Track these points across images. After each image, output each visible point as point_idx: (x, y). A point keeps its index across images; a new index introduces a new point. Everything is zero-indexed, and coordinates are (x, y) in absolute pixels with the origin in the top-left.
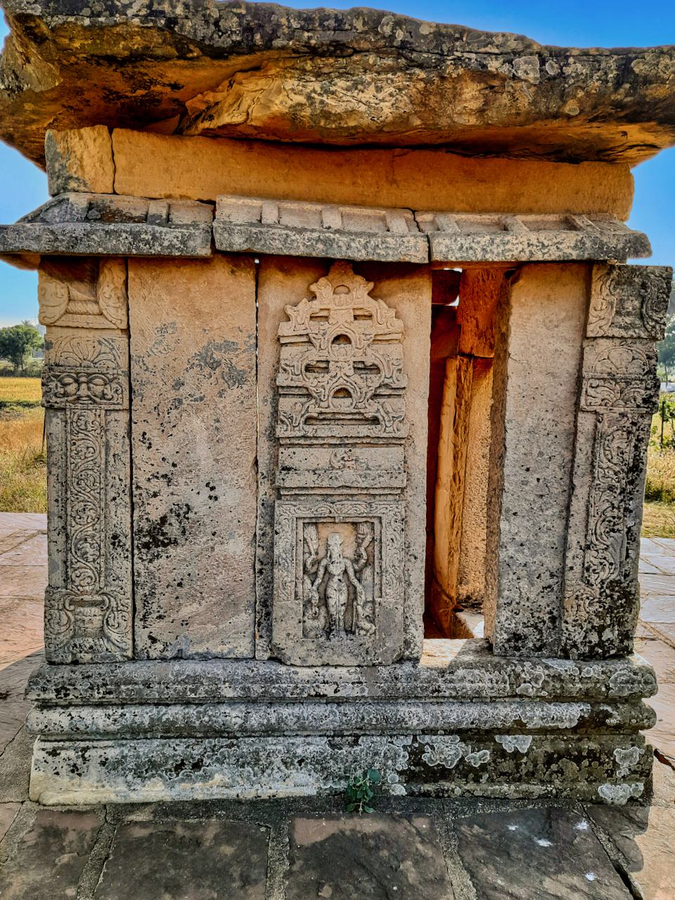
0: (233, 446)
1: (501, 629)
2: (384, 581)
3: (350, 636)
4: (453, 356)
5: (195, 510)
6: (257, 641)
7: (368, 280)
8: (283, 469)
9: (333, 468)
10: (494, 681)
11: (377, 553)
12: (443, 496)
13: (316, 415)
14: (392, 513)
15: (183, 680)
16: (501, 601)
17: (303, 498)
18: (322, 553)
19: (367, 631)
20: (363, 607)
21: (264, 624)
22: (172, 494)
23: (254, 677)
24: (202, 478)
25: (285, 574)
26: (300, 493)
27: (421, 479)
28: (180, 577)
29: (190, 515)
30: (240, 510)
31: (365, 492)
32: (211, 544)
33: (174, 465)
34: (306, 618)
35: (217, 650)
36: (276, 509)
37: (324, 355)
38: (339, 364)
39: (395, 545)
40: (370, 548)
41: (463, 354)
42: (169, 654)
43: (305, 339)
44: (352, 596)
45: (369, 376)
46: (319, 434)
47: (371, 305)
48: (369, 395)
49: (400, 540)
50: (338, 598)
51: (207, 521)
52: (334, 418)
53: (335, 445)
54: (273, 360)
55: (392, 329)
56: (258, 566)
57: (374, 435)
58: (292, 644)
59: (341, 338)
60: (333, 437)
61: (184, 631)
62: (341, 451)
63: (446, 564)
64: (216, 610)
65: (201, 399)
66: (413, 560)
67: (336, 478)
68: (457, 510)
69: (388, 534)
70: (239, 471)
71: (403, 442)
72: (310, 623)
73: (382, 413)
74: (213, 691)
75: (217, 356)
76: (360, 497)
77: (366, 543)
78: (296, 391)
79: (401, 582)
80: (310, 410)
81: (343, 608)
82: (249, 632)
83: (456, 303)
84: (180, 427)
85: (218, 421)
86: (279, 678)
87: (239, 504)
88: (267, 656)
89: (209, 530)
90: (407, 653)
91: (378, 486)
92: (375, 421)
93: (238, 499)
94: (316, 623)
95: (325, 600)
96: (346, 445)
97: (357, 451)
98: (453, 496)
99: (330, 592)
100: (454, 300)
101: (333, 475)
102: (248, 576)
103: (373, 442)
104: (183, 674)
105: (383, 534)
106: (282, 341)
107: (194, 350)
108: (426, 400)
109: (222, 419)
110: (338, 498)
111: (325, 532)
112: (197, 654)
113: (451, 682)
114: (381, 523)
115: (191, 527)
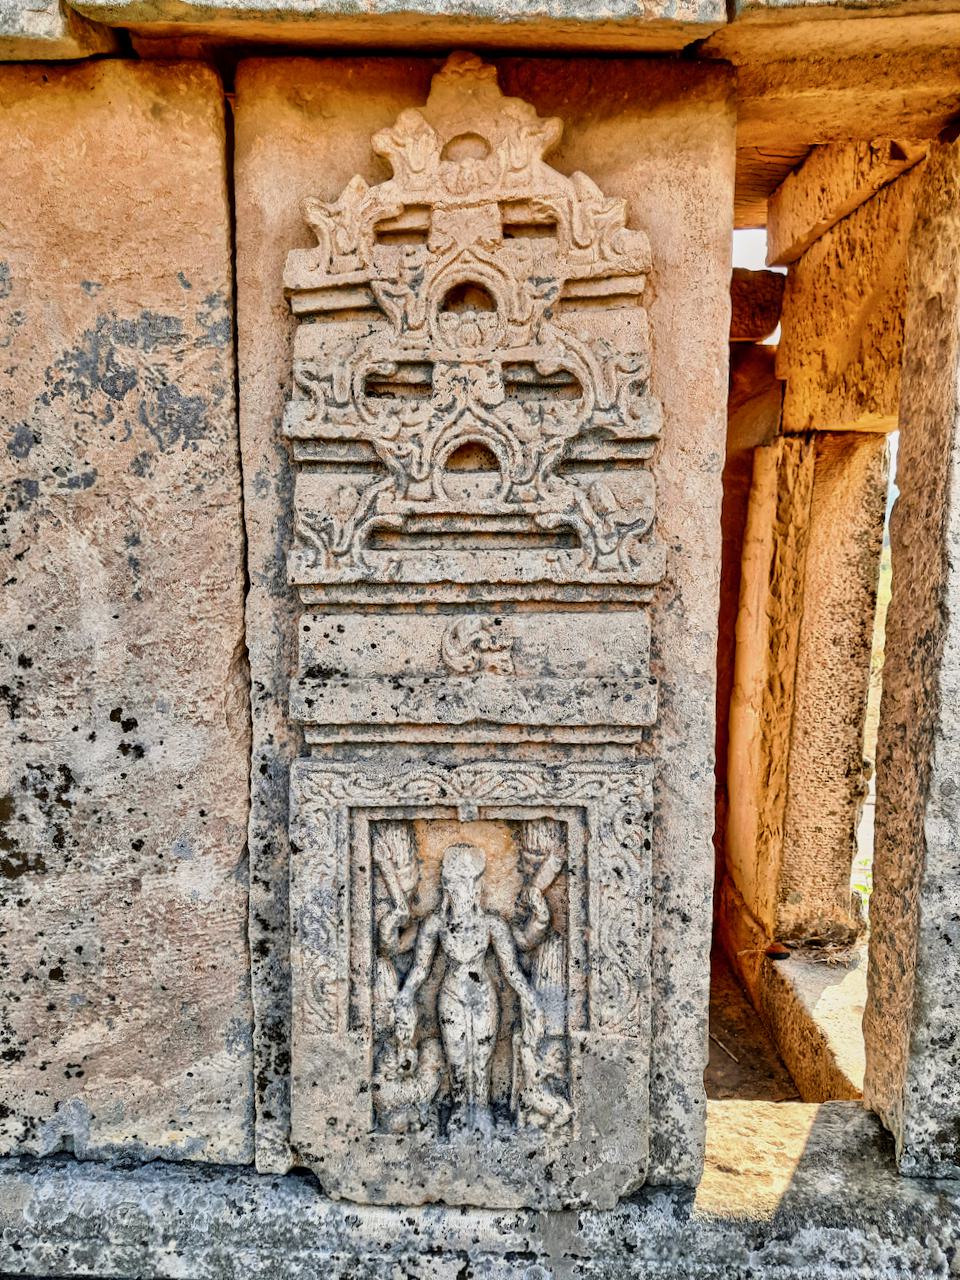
0: (179, 611)
1: (922, 1108)
2: (595, 985)
3: (504, 1129)
4: (768, 441)
5: (85, 783)
6: (259, 1127)
7: (544, 112)
8: (311, 673)
9: (449, 670)
10: (906, 1264)
11: (574, 906)
12: (748, 722)
13: (396, 521)
14: (615, 798)
15: (59, 1228)
16: (924, 1034)
17: (368, 753)
18: (427, 899)
19: (550, 1118)
20: (539, 1052)
21: (276, 1082)
22: (24, 738)
23: (241, 1230)
24: (100, 695)
25: (321, 961)
26: (357, 742)
27: (699, 702)
28: (56, 956)
29: (74, 795)
30: (204, 782)
31: (539, 737)
32: (130, 871)
33: (24, 662)
34: (380, 1079)
35: (160, 1140)
36: (294, 784)
37: (416, 345)
38: (462, 371)
39: (627, 888)
40: (557, 892)
41: (791, 434)
42: (40, 1146)
43: (360, 299)
44: (509, 1016)
45: (548, 405)
46: (409, 574)
47: (549, 188)
48: (549, 460)
49: (642, 870)
50: (469, 1023)
51: (119, 810)
52: (452, 530)
53: (456, 607)
54: (278, 369)
55: (614, 262)
56: (256, 934)
57: (563, 578)
58: (344, 1148)
59: (464, 295)
60: (446, 583)
61: (73, 1093)
62: (470, 624)
63: (753, 857)
64: (154, 1040)
65: (88, 480)
66: (677, 923)
67: (458, 699)
68: (776, 752)
69: (606, 855)
70: (198, 679)
71: (648, 596)
72: (391, 1092)
73: (588, 513)
74: (135, 1262)
75: (125, 357)
76: (528, 752)
77: (545, 878)
78: (341, 454)
79: (642, 988)
80: (380, 506)
81: (485, 1049)
82: (240, 1099)
83: (773, 340)
84: (35, 559)
85: (134, 541)
86: (308, 1236)
87: (200, 768)
88: (283, 1165)
89: (125, 836)
90: (661, 1170)
91: (577, 720)
92: (566, 535)
93: (195, 748)
94: (410, 1090)
95: (433, 1025)
96: (486, 606)
97: (517, 624)
98: (768, 722)
99: (449, 1006)
100: (770, 330)
101: (449, 690)
102: (232, 957)
103: (565, 597)
104: (59, 1211)
105: (593, 856)
106: (302, 305)
107: (60, 344)
108: (717, 478)
109: (146, 537)
110: (465, 754)
111: (434, 843)
112: (110, 1148)
113: (783, 1261)
114: (585, 823)
115: (78, 827)
